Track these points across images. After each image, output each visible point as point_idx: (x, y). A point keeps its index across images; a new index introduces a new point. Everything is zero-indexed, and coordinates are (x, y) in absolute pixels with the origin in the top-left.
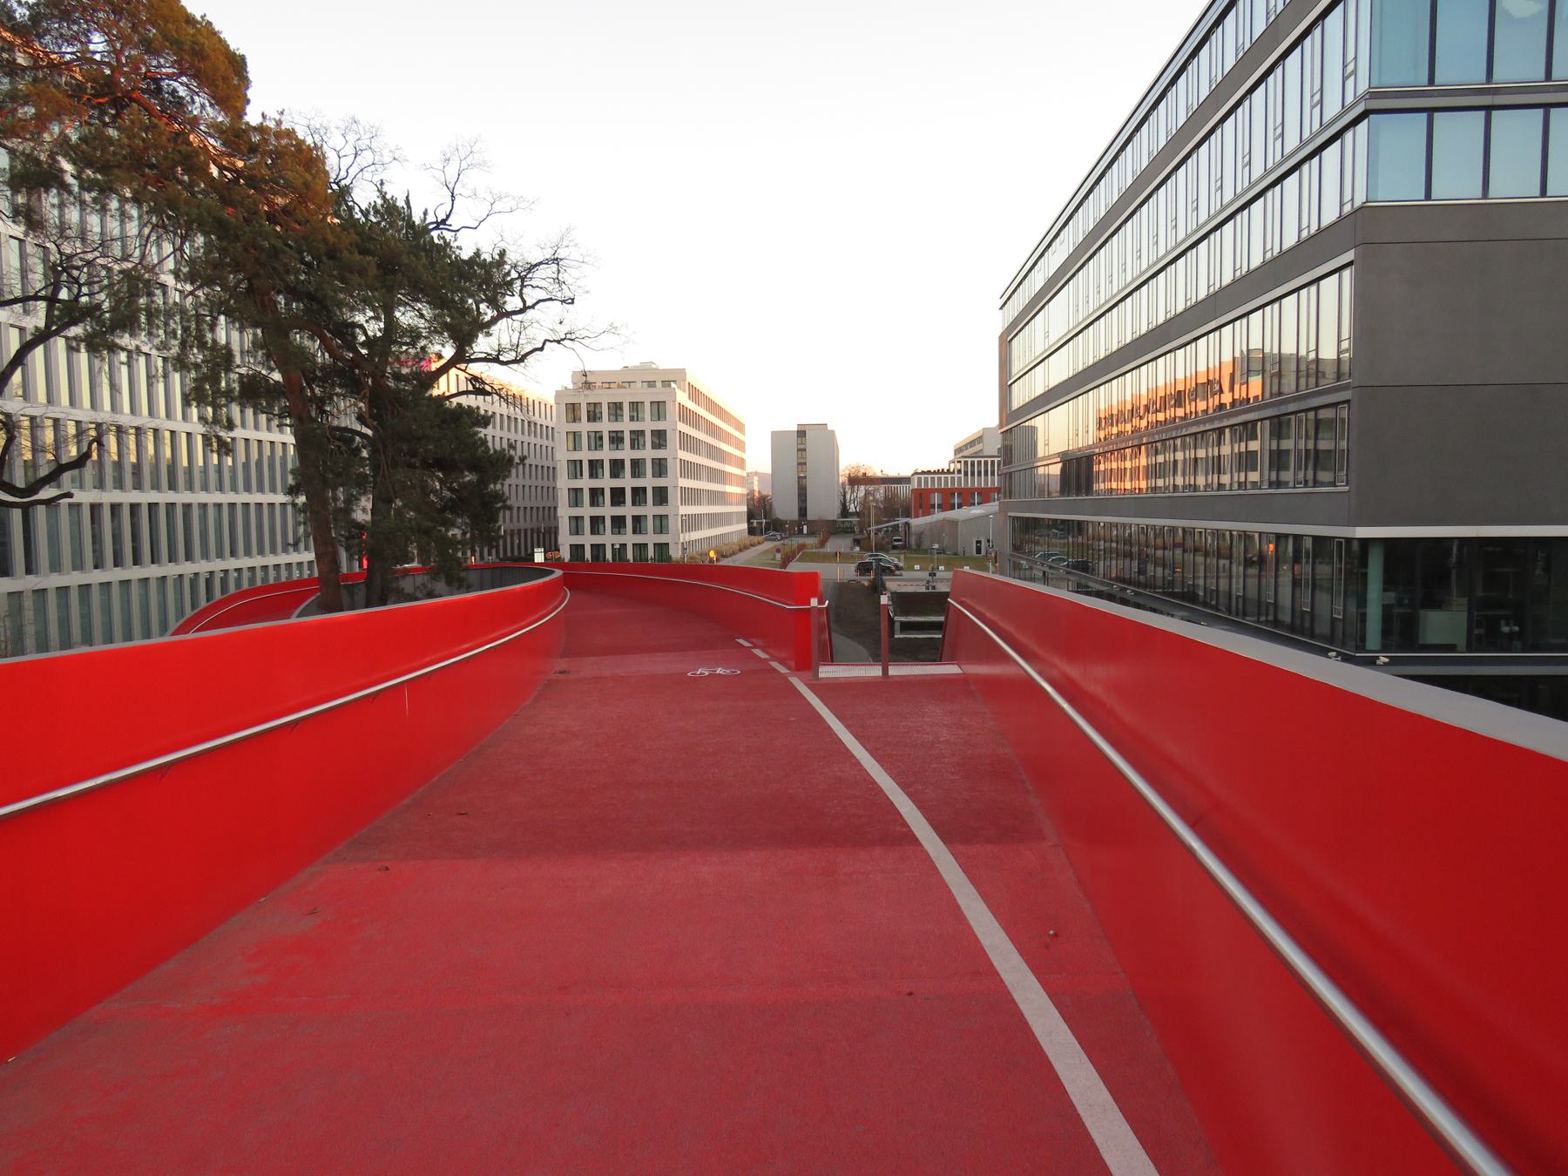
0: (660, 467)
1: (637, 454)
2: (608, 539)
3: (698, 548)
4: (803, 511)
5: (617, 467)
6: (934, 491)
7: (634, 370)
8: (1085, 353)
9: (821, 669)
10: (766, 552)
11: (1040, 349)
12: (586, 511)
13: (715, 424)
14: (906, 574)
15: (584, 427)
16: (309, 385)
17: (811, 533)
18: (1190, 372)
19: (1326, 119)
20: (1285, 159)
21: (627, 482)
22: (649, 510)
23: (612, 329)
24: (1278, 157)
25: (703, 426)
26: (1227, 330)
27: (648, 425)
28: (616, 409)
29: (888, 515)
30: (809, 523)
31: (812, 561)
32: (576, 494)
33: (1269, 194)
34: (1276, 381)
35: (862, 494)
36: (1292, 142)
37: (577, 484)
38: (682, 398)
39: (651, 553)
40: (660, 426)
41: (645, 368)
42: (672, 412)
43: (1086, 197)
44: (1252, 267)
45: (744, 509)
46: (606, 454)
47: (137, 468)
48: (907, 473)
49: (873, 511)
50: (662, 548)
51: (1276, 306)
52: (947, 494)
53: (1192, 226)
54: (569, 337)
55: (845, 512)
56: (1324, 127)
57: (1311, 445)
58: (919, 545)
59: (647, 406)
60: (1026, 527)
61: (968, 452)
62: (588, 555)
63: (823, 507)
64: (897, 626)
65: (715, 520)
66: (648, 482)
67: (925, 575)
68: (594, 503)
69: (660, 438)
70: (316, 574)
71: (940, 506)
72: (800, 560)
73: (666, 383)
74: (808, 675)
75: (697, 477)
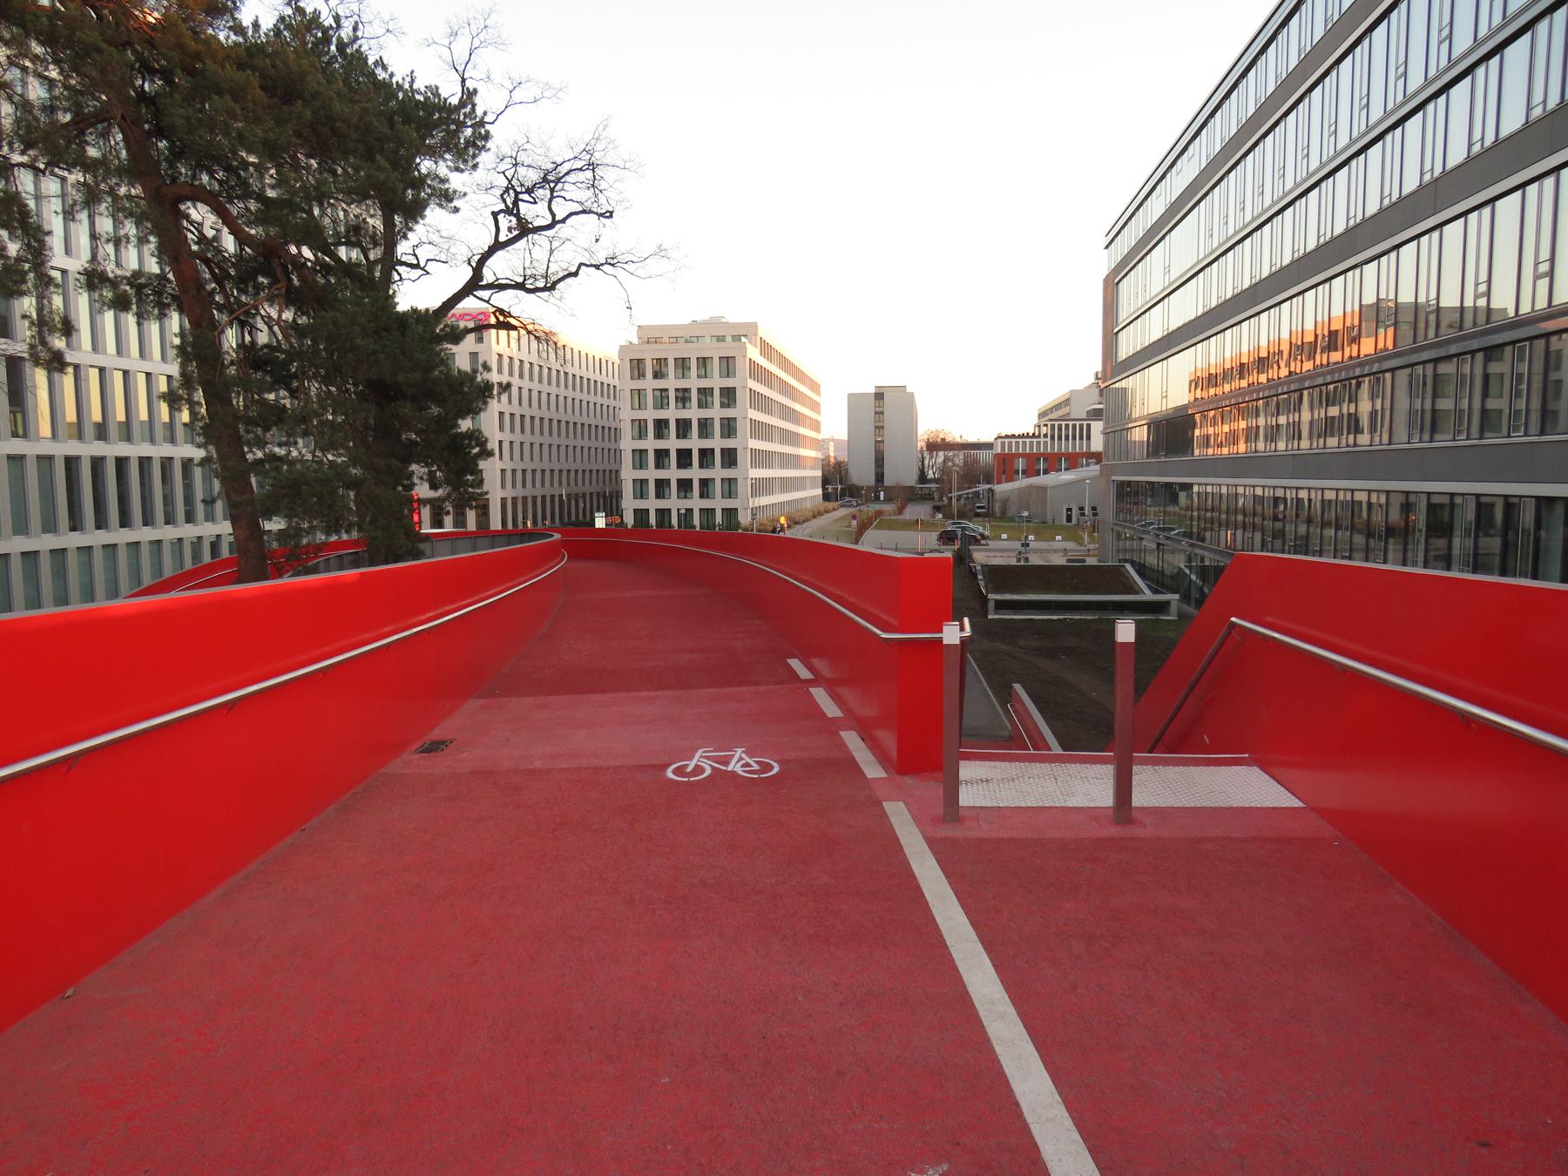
0: (729, 428)
1: (705, 413)
2: (674, 503)
3: (769, 514)
4: (880, 477)
5: (683, 427)
6: (1018, 455)
7: (705, 324)
8: (1143, 333)
9: (967, 770)
10: (841, 519)
11: (1157, 286)
12: (652, 474)
13: (788, 385)
14: (992, 544)
15: (649, 383)
16: (215, 278)
17: (888, 500)
18: (1322, 316)
19: (1410, 91)
20: (1369, 129)
21: (694, 443)
22: (717, 473)
23: (661, 252)
24: (1363, 127)
25: (775, 383)
26: (1310, 295)
27: (716, 382)
28: (682, 364)
29: (966, 483)
30: (887, 490)
31: (890, 528)
32: (640, 454)
33: (1354, 163)
34: (1543, 284)
35: (940, 459)
36: (1376, 113)
37: (641, 445)
38: (753, 353)
39: (719, 519)
40: (729, 383)
41: (715, 323)
42: (742, 368)
43: (1227, 96)
44: (1336, 233)
45: (819, 473)
46: (672, 413)
47: (127, 424)
48: (988, 437)
49: (955, 477)
50: (730, 513)
51: (1436, 235)
52: (1032, 459)
53: (1278, 193)
54: (611, 262)
55: (923, 478)
56: (1452, 64)
57: (1428, 406)
58: (1003, 513)
59: (716, 361)
60: (1127, 493)
61: (1057, 417)
62: (652, 520)
63: (901, 473)
64: (991, 605)
65: (787, 484)
66: (717, 443)
67: (1017, 545)
68: (659, 465)
69: (729, 396)
70: (225, 553)
71: (1024, 472)
72: (878, 527)
73: (736, 338)
74: (929, 789)
75: (769, 439)
